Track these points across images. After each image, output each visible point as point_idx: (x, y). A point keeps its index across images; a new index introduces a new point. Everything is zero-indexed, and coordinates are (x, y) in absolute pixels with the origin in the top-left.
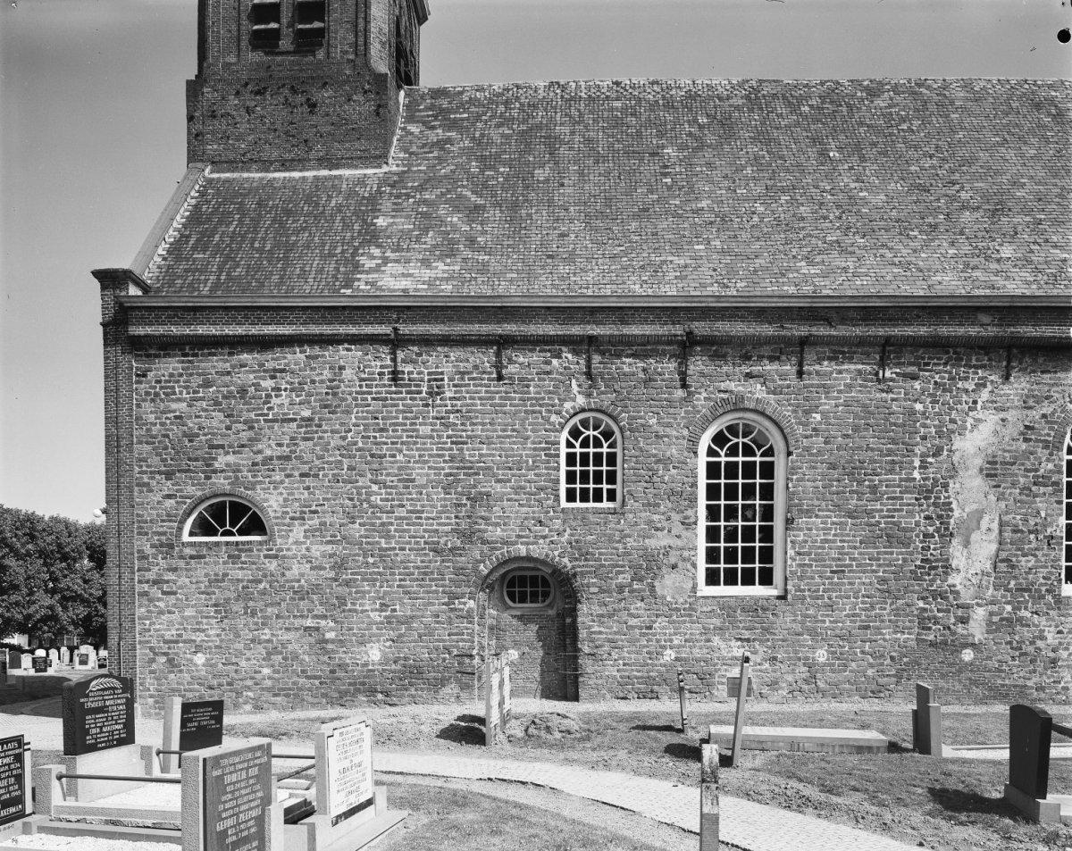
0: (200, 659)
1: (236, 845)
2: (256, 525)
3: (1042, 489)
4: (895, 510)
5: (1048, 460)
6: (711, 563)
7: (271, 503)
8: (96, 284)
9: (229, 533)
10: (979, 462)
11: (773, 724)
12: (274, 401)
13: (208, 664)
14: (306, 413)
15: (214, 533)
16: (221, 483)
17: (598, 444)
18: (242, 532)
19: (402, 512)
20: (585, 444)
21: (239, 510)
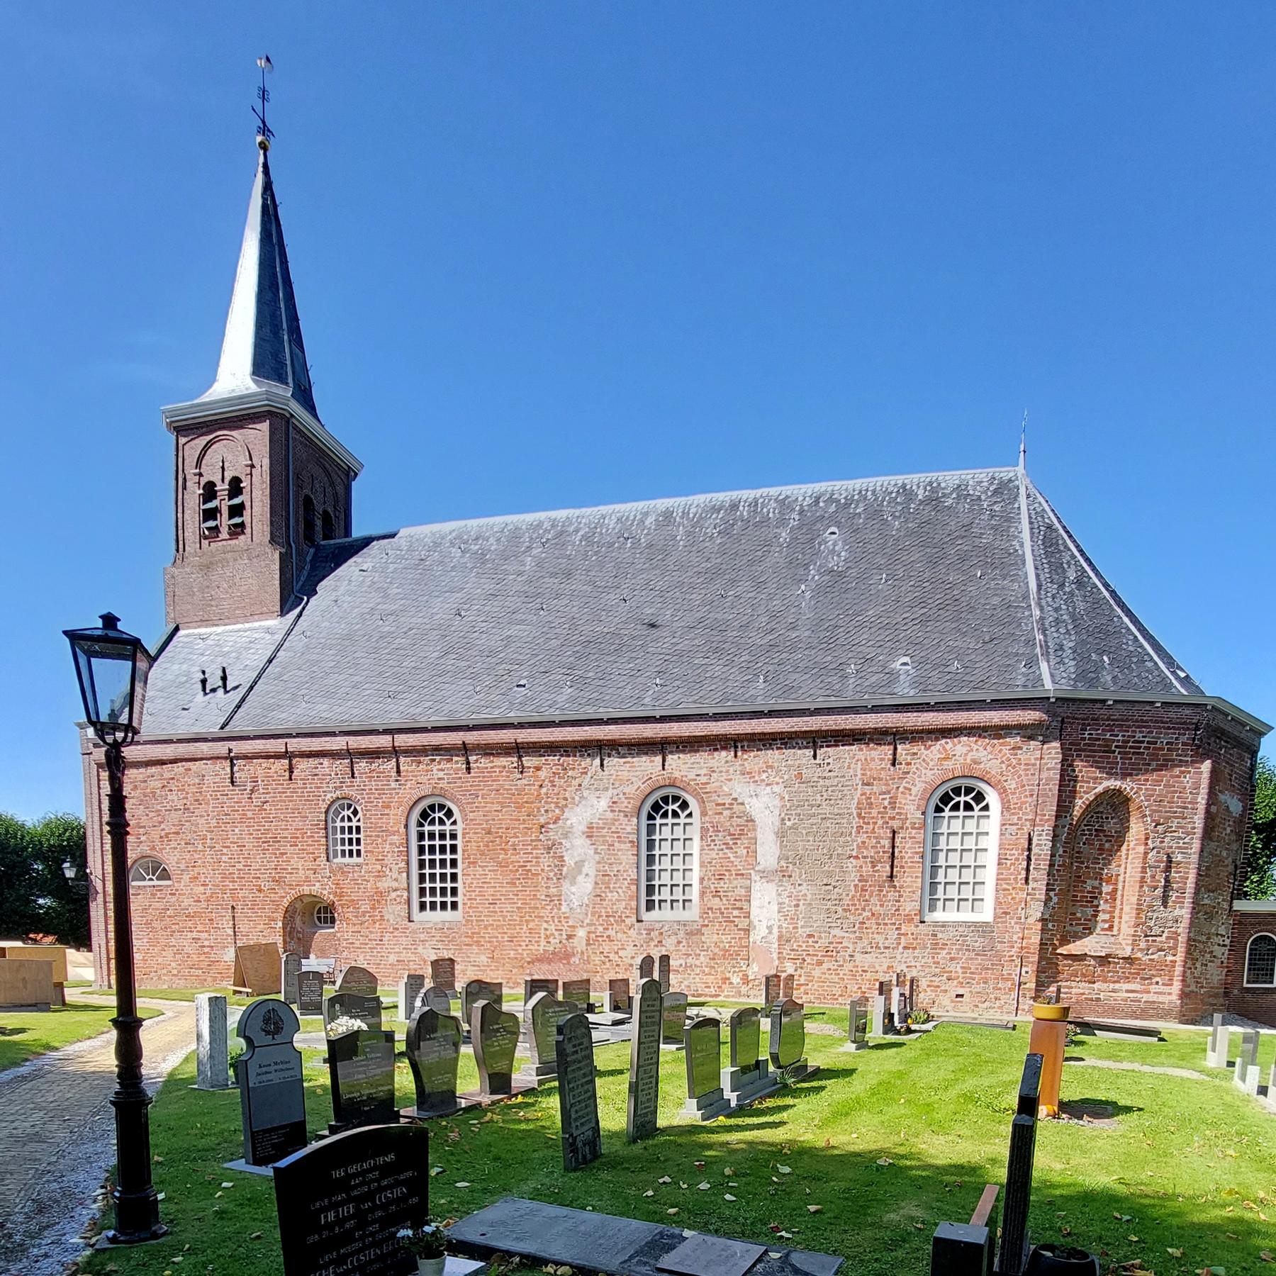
2: (165, 875)
3: (623, 846)
10: (583, 828)
20: (343, 820)
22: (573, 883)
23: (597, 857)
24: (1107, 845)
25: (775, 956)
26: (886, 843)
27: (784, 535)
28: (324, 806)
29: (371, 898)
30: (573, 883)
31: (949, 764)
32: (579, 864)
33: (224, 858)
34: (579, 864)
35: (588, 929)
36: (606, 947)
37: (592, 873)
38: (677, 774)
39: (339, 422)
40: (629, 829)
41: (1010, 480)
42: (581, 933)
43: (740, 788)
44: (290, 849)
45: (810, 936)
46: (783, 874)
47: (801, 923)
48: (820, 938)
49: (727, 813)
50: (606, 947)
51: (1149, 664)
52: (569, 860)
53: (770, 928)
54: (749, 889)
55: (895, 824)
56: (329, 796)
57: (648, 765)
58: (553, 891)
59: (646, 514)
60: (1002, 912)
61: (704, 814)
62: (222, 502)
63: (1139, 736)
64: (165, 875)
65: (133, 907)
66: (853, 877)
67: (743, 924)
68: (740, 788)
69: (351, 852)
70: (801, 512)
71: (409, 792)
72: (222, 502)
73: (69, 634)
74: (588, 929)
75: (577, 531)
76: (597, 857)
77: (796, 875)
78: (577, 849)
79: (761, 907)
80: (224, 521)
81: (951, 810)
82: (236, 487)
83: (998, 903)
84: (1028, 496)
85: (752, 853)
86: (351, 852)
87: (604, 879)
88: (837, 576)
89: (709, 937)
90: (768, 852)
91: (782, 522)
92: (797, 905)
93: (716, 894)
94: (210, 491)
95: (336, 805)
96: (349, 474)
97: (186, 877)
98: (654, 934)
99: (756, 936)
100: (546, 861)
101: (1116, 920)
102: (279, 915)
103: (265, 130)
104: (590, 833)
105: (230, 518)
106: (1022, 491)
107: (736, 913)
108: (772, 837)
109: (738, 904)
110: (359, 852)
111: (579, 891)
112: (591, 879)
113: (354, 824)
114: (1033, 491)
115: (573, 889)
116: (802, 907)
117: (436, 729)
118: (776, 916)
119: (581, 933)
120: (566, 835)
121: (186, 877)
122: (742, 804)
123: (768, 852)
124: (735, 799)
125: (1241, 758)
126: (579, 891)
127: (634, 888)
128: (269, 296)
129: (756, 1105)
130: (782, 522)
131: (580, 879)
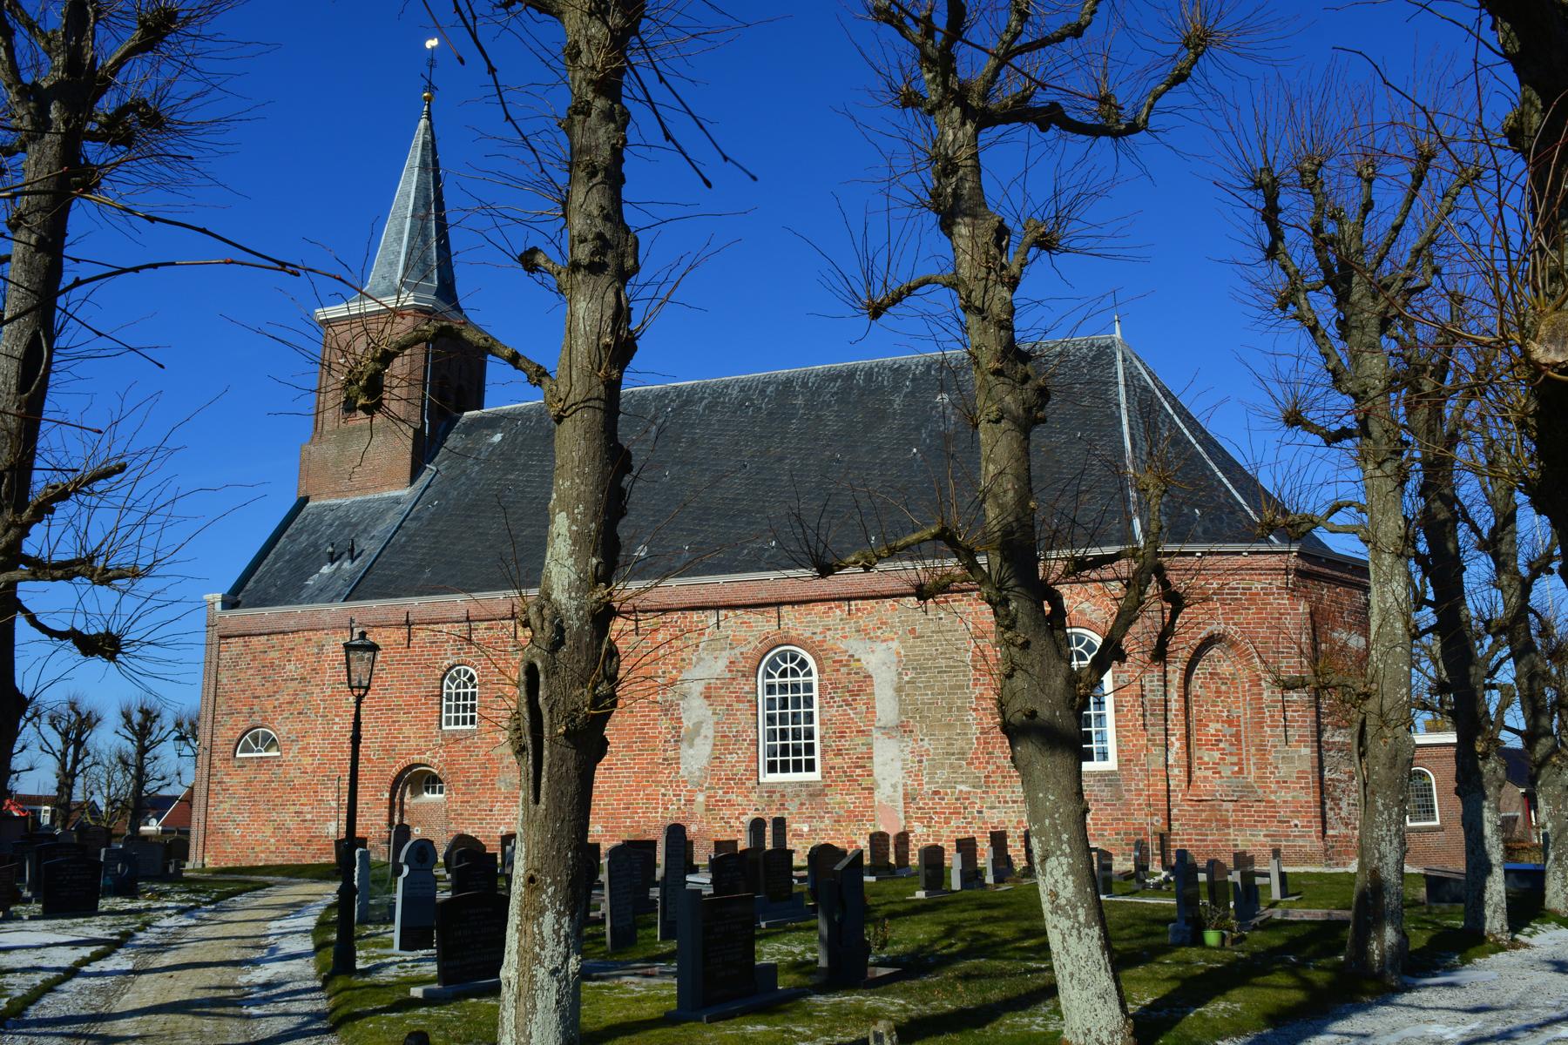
3: (741, 706)
17: (466, 686)
22: (691, 746)
23: (715, 718)
24: (1224, 688)
25: (902, 816)
27: (898, 402)
28: (439, 673)
29: (483, 766)
30: (691, 746)
32: (698, 726)
33: (336, 728)
34: (698, 726)
35: (708, 793)
36: (726, 812)
37: (711, 733)
38: (793, 633)
40: (747, 688)
41: (1108, 347)
42: (700, 798)
43: (855, 646)
44: (402, 717)
45: (936, 793)
46: (903, 729)
47: (926, 779)
49: (843, 670)
50: (726, 812)
51: (1241, 515)
52: (687, 723)
53: (894, 786)
54: (870, 746)
57: (763, 624)
58: (670, 754)
59: (769, 383)
60: (1125, 761)
61: (821, 671)
63: (1233, 584)
66: (975, 730)
67: (866, 783)
68: (855, 646)
69: (464, 718)
70: (913, 380)
74: (708, 793)
75: (702, 399)
76: (715, 718)
77: (917, 731)
78: (695, 710)
79: (885, 764)
83: (1120, 751)
84: (1124, 360)
85: (870, 708)
86: (464, 718)
87: (724, 742)
88: (946, 438)
89: (834, 799)
90: (886, 707)
91: (896, 388)
92: (920, 761)
93: (839, 753)
95: (453, 671)
97: (295, 748)
98: (776, 797)
99: (879, 796)
100: (664, 724)
102: (387, 787)
103: (431, 87)
106: (1119, 356)
107: (859, 771)
108: (890, 693)
109: (861, 762)
110: (472, 718)
111: (696, 757)
112: (710, 741)
113: (469, 690)
114: (1129, 354)
115: (691, 752)
116: (925, 763)
118: (900, 774)
119: (700, 798)
120: (684, 696)
121: (295, 748)
123: (886, 707)
126: (696, 757)
127: (753, 749)
128: (422, 213)
130: (896, 388)
131: (698, 741)
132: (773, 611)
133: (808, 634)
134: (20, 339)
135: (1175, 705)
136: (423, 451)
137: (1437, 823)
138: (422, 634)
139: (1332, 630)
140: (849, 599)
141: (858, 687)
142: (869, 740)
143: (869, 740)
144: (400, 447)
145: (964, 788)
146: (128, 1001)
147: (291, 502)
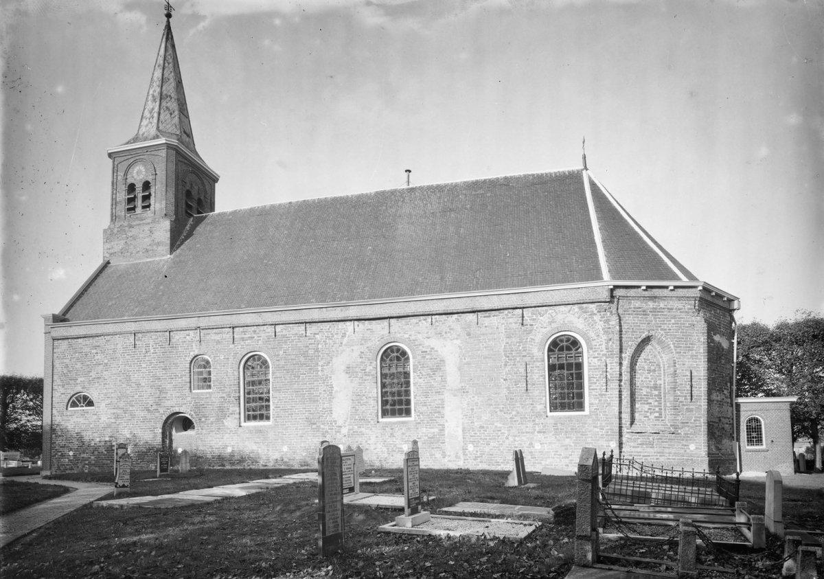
0: (71, 453)
1: (383, 578)
2: (90, 403)
3: (368, 378)
4: (312, 388)
5: (370, 365)
6: (619, 279)
7: (93, 394)
8: (43, 320)
9: (83, 406)
10: (343, 367)
11: (737, 427)
12: (96, 357)
13: (74, 455)
14: (106, 361)
15: (78, 406)
16: (79, 389)
18: (86, 406)
19: (136, 397)
21: (85, 398)
26: (522, 370)
31: (554, 325)
39: (209, 153)
43: (434, 343)
45: (482, 427)
46: (463, 391)
48: (488, 427)
55: (527, 359)
56: (192, 353)
62: (140, 194)
64: (90, 403)
65: (436, 466)
68: (434, 343)
71: (242, 349)
72: (140, 194)
73: (110, 155)
80: (139, 203)
81: (559, 350)
82: (147, 185)
85: (444, 380)
87: (358, 398)
90: (453, 376)
94: (132, 188)
96: (214, 179)
101: (663, 411)
102: (160, 425)
104: (349, 370)
105: (143, 202)
117: (621, 206)
122: (437, 351)
124: (433, 349)
125: (724, 316)
129: (595, 566)
132: (386, 322)
133: (406, 336)
134: (302, 466)
135: (626, 377)
136: (177, 238)
137: (764, 447)
138: (177, 337)
139: (715, 334)
140: (432, 315)
141: (438, 367)
142: (442, 397)
143: (442, 397)
144: (163, 229)
145: (499, 425)
146: (513, 479)
147: (99, 263)
